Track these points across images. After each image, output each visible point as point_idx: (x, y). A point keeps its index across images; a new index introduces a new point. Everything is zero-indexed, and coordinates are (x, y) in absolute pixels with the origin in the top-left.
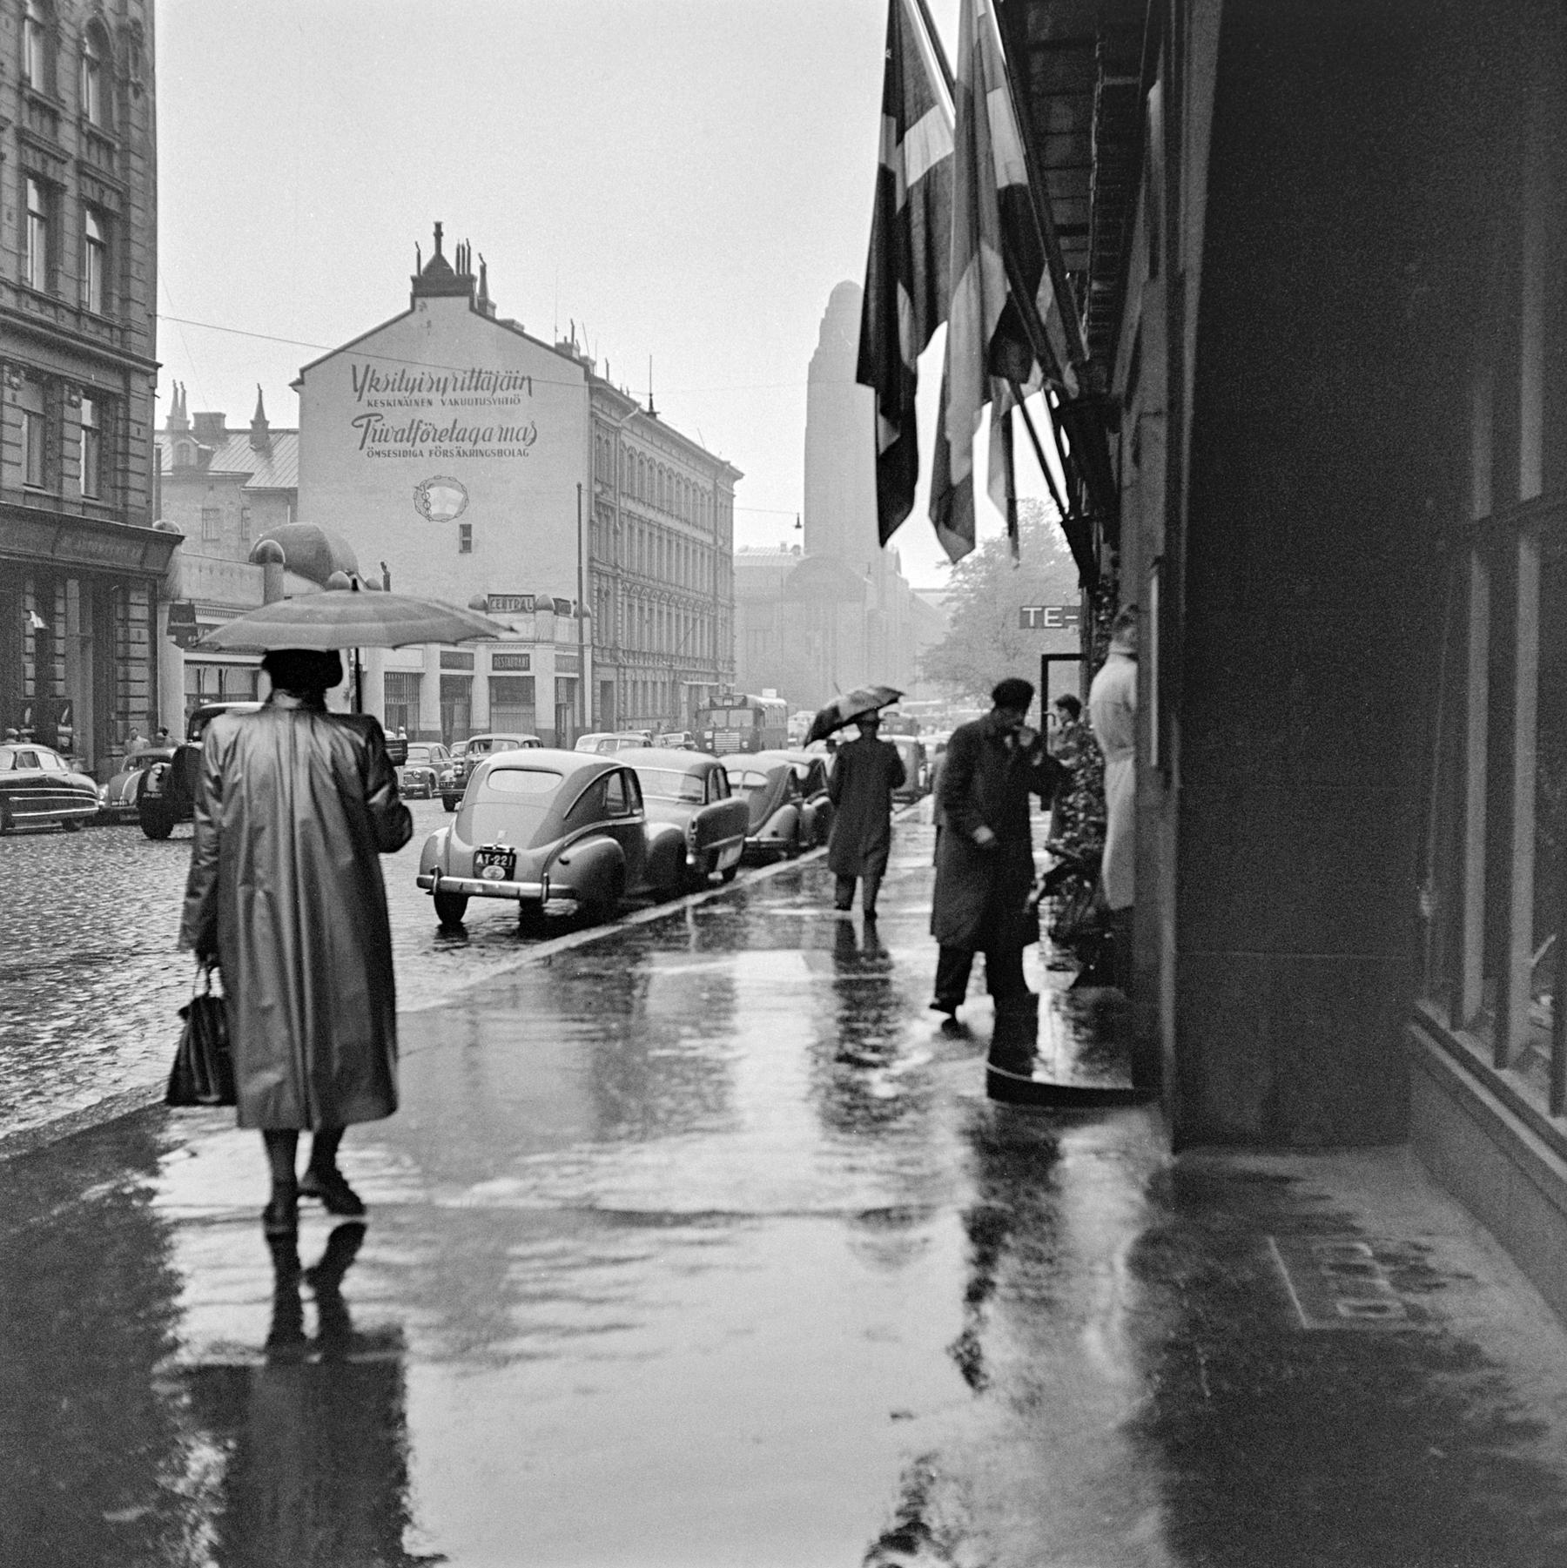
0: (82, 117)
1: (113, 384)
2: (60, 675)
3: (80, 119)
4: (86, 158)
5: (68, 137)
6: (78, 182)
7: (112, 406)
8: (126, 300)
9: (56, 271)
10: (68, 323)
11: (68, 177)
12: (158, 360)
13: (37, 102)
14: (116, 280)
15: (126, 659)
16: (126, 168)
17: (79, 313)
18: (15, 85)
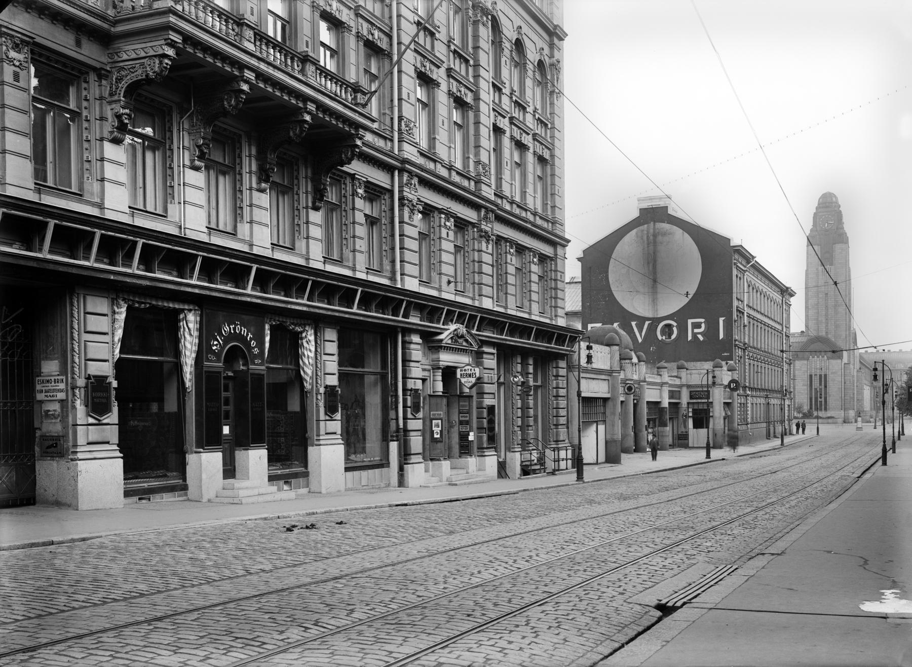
0: (450, 41)
1: (547, 250)
2: (531, 405)
3: (449, 42)
4: (452, 66)
5: (441, 50)
6: (511, 129)
7: (503, 245)
8: (553, 207)
9: (435, 138)
10: (444, 172)
11: (439, 75)
12: (567, 236)
13: (458, 53)
14: (472, 150)
15: (557, 396)
16: (477, 76)
17: (450, 168)
18: (446, 42)
